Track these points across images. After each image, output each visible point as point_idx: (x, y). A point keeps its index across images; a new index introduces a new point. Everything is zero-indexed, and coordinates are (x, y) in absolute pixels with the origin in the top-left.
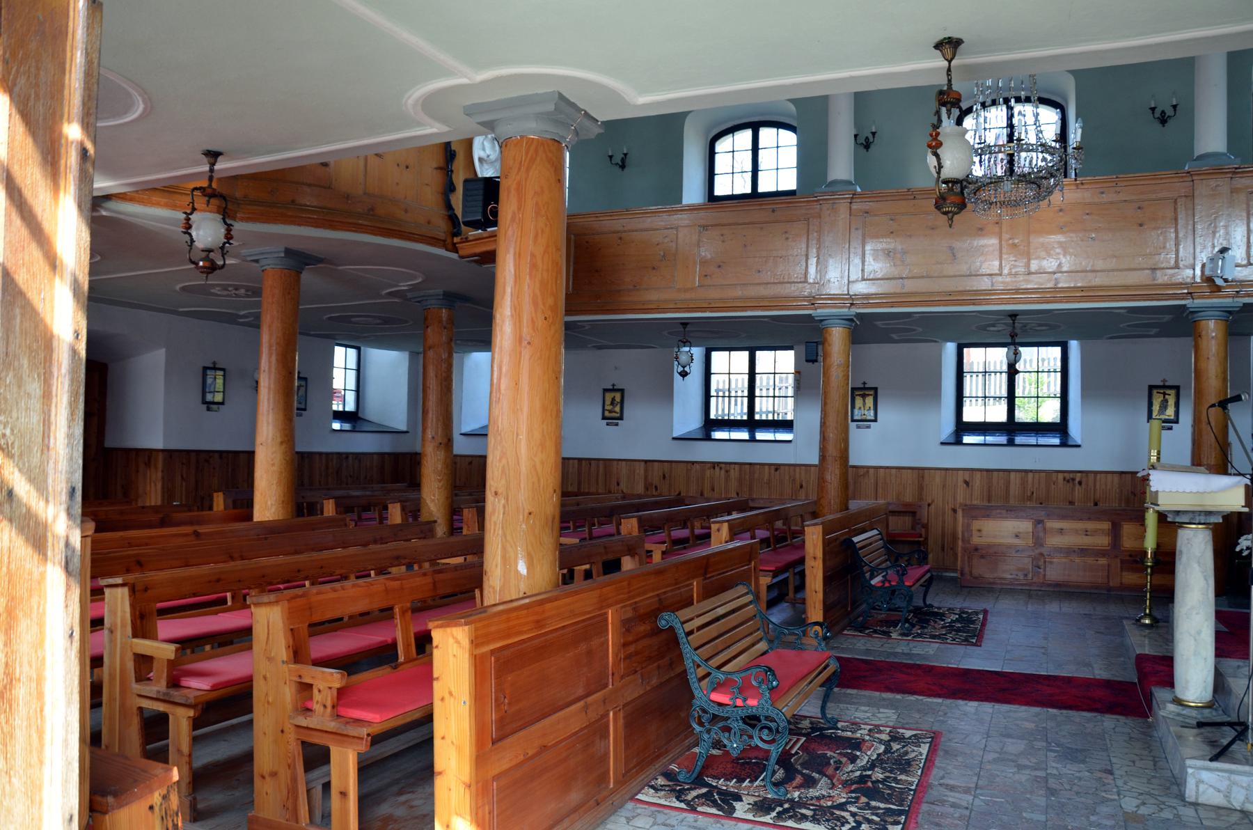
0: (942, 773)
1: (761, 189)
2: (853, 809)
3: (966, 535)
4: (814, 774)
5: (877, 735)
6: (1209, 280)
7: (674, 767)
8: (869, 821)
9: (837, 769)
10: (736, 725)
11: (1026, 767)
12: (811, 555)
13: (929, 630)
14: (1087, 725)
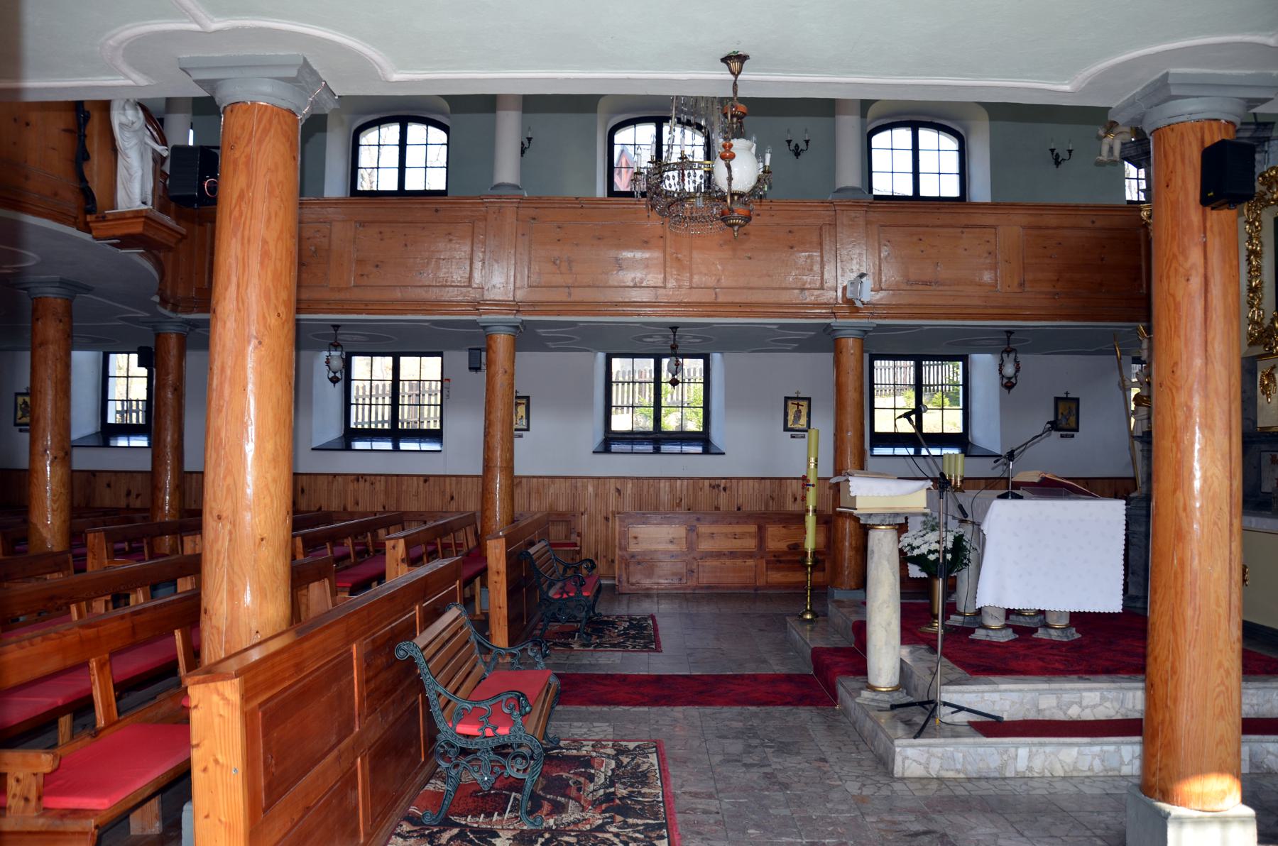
0: (680, 782)
1: (408, 187)
2: (615, 830)
3: (623, 541)
4: (559, 798)
5: (602, 750)
6: (850, 303)
7: (413, 809)
8: (635, 840)
9: (579, 790)
10: (487, 757)
11: (752, 765)
12: (494, 570)
13: (606, 639)
14: (788, 719)
